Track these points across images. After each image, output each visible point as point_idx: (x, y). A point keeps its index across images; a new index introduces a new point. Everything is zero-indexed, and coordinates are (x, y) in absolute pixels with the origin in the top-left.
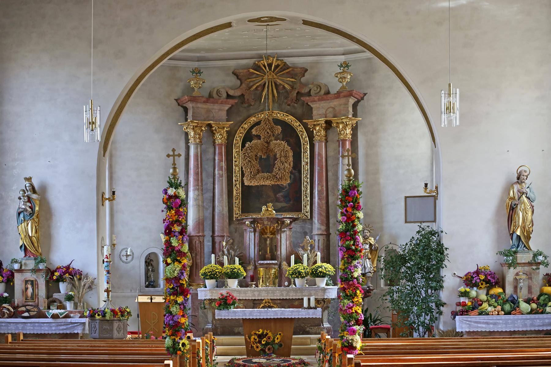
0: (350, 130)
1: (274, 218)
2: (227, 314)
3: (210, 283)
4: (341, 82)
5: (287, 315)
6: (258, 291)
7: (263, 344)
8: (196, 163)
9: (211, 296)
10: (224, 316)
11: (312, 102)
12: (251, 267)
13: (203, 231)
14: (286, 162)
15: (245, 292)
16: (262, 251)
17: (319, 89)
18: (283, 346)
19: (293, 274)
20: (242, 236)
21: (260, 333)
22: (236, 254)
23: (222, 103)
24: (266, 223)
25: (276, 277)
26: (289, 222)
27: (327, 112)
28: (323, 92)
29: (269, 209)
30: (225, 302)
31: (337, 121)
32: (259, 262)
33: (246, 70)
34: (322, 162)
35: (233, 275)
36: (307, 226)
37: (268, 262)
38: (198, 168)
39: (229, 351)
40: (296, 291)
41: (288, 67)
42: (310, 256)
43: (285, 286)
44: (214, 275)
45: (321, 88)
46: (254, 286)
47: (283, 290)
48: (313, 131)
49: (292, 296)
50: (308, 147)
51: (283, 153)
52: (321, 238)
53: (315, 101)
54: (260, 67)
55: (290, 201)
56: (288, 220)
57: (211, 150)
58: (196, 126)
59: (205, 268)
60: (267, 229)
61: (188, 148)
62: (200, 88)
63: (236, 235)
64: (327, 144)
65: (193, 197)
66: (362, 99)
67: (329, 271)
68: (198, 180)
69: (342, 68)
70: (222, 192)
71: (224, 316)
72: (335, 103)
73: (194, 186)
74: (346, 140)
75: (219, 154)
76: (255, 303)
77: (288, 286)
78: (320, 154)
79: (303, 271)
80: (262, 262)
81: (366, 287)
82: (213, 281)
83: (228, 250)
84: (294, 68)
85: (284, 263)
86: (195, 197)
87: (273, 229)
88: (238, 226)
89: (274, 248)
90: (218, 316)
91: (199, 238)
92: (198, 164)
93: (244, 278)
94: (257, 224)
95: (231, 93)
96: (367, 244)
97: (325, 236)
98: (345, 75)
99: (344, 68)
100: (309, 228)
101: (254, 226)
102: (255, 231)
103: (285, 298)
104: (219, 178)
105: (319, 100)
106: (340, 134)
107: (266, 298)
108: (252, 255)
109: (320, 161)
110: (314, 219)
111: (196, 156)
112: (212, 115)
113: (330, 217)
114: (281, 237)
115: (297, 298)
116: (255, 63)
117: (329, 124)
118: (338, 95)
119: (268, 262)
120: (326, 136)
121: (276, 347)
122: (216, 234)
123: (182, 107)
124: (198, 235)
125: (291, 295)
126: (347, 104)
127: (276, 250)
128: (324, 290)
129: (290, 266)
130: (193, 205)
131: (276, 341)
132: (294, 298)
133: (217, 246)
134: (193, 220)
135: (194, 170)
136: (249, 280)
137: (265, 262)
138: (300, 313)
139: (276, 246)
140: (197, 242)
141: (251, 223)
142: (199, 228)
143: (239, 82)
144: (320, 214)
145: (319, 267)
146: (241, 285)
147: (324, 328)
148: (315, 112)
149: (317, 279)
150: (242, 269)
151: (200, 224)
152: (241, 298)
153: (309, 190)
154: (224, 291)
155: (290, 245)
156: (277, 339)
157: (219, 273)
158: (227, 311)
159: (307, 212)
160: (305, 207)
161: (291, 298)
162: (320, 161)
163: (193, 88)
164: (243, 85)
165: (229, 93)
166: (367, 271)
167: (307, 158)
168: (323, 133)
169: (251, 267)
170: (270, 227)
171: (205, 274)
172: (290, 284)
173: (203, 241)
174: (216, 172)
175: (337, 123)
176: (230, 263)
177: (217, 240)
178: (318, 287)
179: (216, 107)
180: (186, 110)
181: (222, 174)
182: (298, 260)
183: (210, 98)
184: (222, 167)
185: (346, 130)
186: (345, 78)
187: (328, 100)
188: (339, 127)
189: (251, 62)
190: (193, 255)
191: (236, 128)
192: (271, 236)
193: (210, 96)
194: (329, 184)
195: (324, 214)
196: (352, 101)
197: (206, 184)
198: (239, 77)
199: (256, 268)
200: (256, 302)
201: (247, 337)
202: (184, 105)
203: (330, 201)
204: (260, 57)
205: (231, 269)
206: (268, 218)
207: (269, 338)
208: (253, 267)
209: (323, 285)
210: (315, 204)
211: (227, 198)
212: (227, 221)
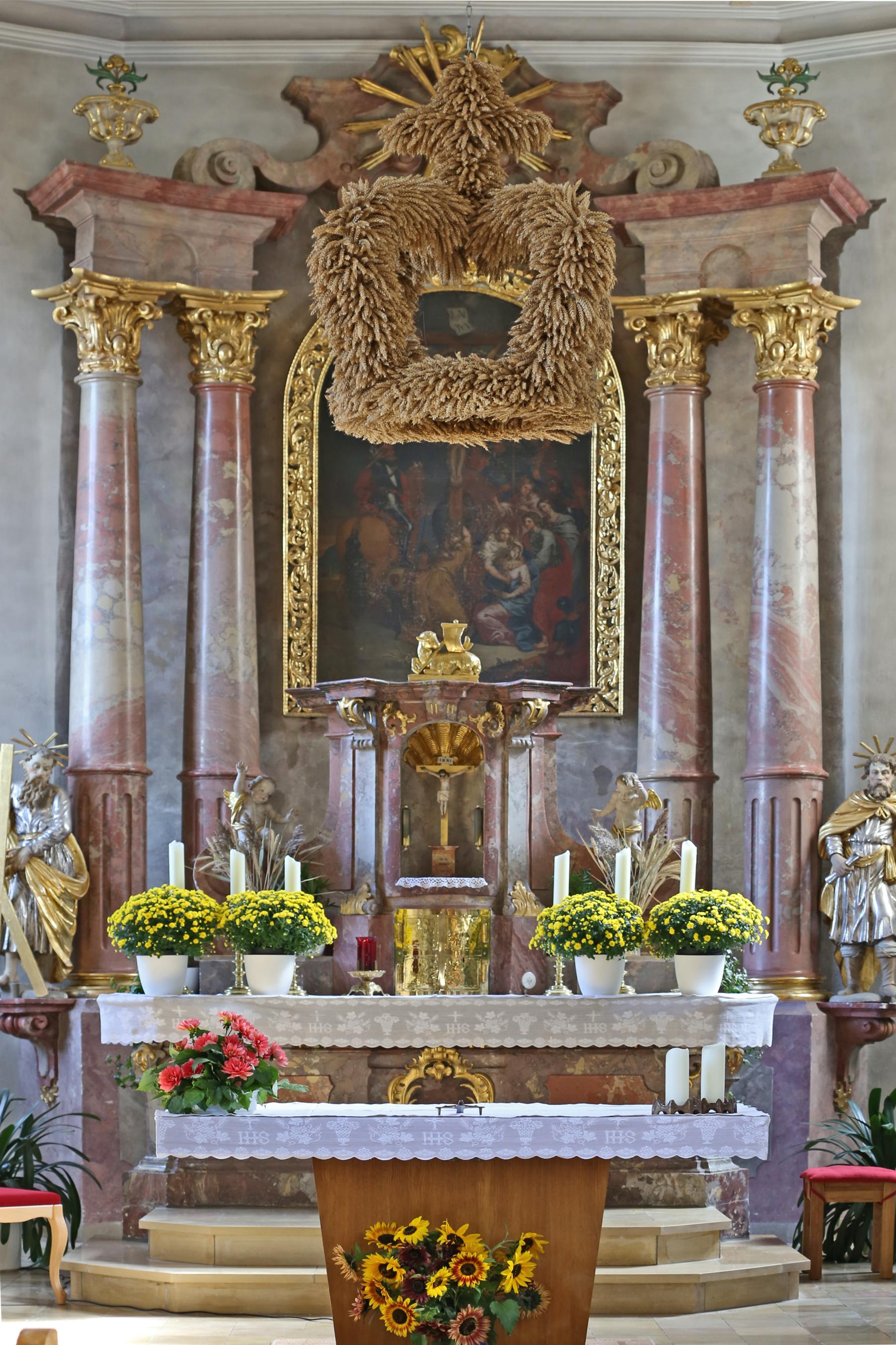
0: (812, 342)
1: (471, 688)
2: (223, 1137)
3: (154, 970)
4: (772, 144)
5: (574, 1145)
6: (393, 1010)
7: (434, 1301)
8: (110, 459)
9: (161, 1030)
10: (208, 1145)
11: (642, 218)
12: (358, 906)
13: (141, 751)
14: (585, 292)
15: (330, 1016)
16: (417, 835)
17: (673, 170)
18: (545, 1304)
19: (566, 935)
20: (320, 776)
21: (415, 1238)
22: (291, 845)
23: (231, 208)
24: (434, 706)
25: (480, 952)
26: (544, 706)
27: (711, 266)
28: (690, 180)
29: (452, 648)
30: (215, 1072)
31: (756, 304)
32: (401, 882)
33: (344, 85)
34: (685, 477)
35: (272, 936)
36: (609, 743)
37: (444, 882)
38: (119, 482)
39: (246, 1296)
40: (580, 1013)
41: (535, 81)
42: (641, 858)
43: (522, 991)
44: (178, 934)
45: (681, 166)
46: (374, 987)
47: (511, 1012)
48: (643, 346)
49: (562, 1036)
50: (621, 417)
51: (566, 237)
52: (677, 794)
53: (657, 217)
54: (406, 72)
55: (539, 640)
56: (540, 696)
57: (184, 416)
58: (110, 301)
59: (133, 901)
60: (437, 738)
61: (74, 397)
62: (131, 141)
63: (295, 777)
64: (708, 402)
65: (96, 607)
66: (864, 222)
67: (742, 926)
68: (121, 533)
69: (776, 87)
70: (232, 588)
71: (208, 1145)
72: (748, 226)
73: (99, 559)
74: (794, 384)
75: (216, 426)
76: (374, 1071)
77: (540, 989)
78: (674, 444)
79: (616, 924)
80: (413, 882)
81: (875, 997)
82: (174, 964)
83: (251, 829)
84: (562, 84)
85: (521, 893)
86: (106, 604)
87: (470, 736)
88: (301, 740)
89: (471, 823)
90: (168, 1144)
91: (122, 782)
92: (118, 466)
93: (329, 950)
94: (392, 712)
95: (275, 173)
96: (882, 820)
97: (691, 786)
98: (793, 114)
99: (788, 84)
100: (618, 755)
101: (379, 720)
102: (381, 744)
103: (524, 1043)
104: (214, 529)
105: (676, 212)
106: (765, 357)
107: (434, 1043)
108: (367, 851)
109: (675, 473)
110: (642, 715)
111: (113, 430)
112: (184, 260)
113: (715, 710)
114: (505, 775)
115: (586, 1043)
116: (384, 57)
117: (716, 316)
118: (760, 194)
119: (444, 882)
120: (702, 369)
121: (510, 1312)
122: (202, 766)
123: (52, 223)
124: (117, 766)
125: (555, 1030)
126: (798, 232)
127: (482, 830)
128: (717, 1012)
129: (547, 901)
130: (96, 641)
131: (510, 1283)
132: (570, 1043)
133: (205, 817)
134: (94, 705)
135: (99, 487)
136: (349, 959)
137: (430, 883)
138: (648, 1136)
139: (482, 814)
140: (114, 797)
141: (365, 705)
142: (122, 738)
143: (311, 134)
144: (671, 693)
145: (693, 907)
146: (311, 981)
147: (710, 1179)
148: (653, 266)
149: (683, 963)
150: (317, 911)
151: (127, 722)
152: (311, 1042)
153: (621, 597)
154: (212, 1014)
155: (549, 811)
156: (517, 1270)
157: (202, 922)
158: (224, 1119)
159: (610, 688)
160: (605, 664)
161: (554, 1043)
162: (675, 473)
163: (100, 140)
164: (332, 145)
165: (267, 173)
166: (880, 932)
167: (616, 464)
168: (689, 352)
169: (358, 906)
170: (455, 729)
171: (133, 930)
172: (544, 984)
173: (143, 796)
174: (205, 504)
175: (757, 311)
176: (257, 884)
177: (204, 790)
178: (688, 995)
179: (207, 224)
180: (67, 236)
181: (233, 515)
182: (589, 876)
183: (174, 187)
184: (232, 482)
185: (793, 340)
186: (789, 124)
187: (718, 212)
188: (762, 330)
189: (368, 52)
190: (96, 853)
191: (298, 327)
192: (459, 769)
193: (181, 173)
194: (712, 573)
195: (691, 695)
196: (822, 221)
197: (160, 559)
198: (314, 112)
199: (383, 908)
200: (382, 1060)
201: (341, 1260)
202: (58, 213)
203: (715, 645)
204: (410, 32)
205: (264, 907)
206: (444, 685)
207: (469, 1266)
208: (372, 906)
209: (710, 988)
210: (649, 649)
211: (252, 616)
212: (254, 712)
